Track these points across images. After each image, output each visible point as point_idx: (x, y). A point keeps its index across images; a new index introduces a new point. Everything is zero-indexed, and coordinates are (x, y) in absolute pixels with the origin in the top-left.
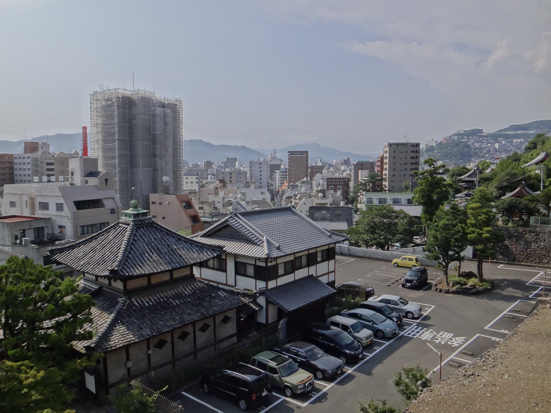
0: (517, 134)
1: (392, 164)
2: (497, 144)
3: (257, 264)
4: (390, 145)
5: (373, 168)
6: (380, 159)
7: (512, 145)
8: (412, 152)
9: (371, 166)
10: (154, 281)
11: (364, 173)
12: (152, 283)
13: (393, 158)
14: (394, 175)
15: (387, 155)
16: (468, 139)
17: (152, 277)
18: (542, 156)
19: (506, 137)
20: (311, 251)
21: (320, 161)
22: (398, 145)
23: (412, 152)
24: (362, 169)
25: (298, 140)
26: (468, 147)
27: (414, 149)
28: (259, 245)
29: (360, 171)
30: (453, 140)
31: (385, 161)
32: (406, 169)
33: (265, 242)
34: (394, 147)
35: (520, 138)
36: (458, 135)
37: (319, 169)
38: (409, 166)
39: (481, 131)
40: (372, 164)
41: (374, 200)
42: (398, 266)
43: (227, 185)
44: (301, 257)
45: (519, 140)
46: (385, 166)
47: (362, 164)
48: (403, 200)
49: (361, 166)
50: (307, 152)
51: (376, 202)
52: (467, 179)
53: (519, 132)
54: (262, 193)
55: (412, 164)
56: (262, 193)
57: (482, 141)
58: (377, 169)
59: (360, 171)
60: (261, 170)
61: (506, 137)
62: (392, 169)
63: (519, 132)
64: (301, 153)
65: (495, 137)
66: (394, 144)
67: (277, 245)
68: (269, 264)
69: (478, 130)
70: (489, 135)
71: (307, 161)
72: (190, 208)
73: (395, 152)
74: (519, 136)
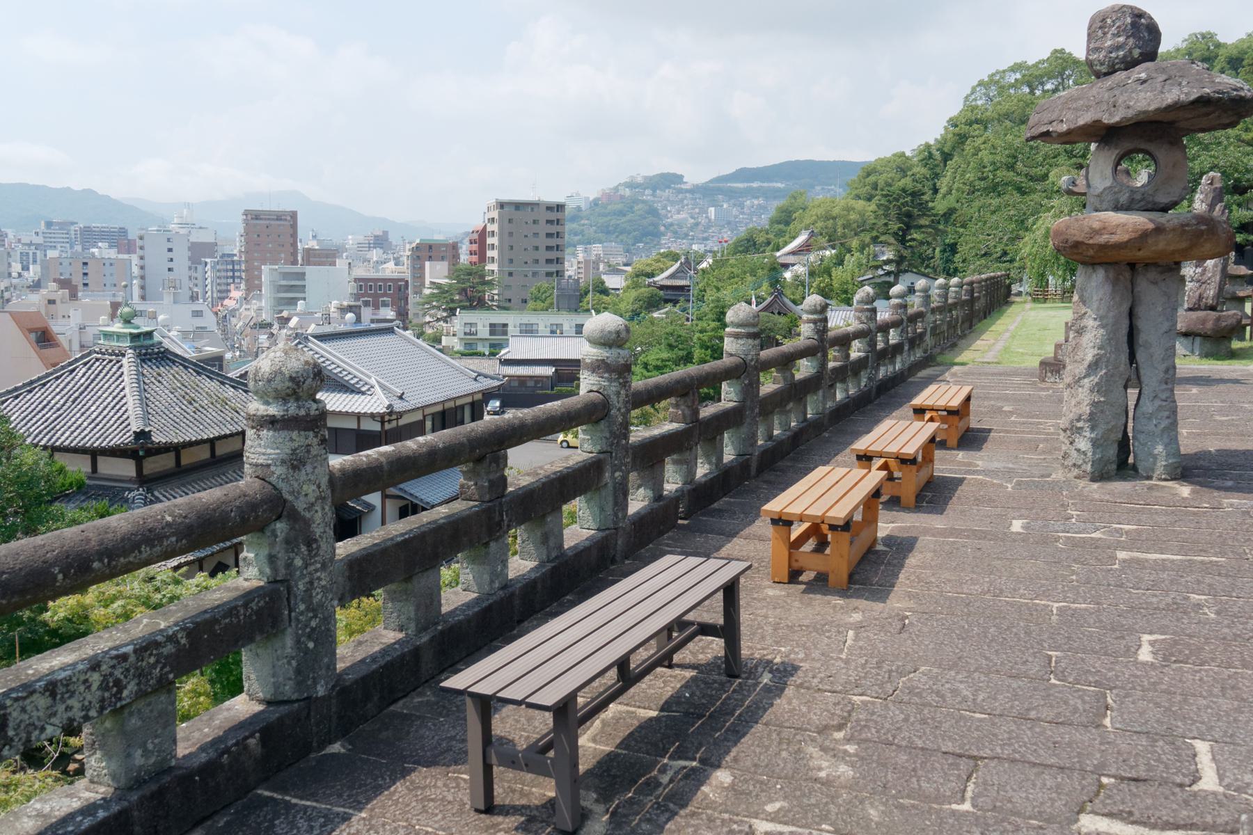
0: (751, 189)
1: (508, 248)
2: (712, 209)
3: (362, 427)
4: (502, 205)
5: (456, 256)
6: (476, 236)
7: (743, 213)
8: (548, 222)
9: (446, 251)
10: (187, 458)
11: (438, 267)
12: (145, 472)
13: (508, 234)
14: (511, 274)
15: (494, 227)
16: (654, 195)
17: (218, 443)
18: (802, 238)
19: (732, 194)
20: (448, 405)
21: (314, 237)
22: (518, 206)
23: (548, 222)
24: (430, 258)
25: (269, 188)
26: (653, 212)
27: (553, 216)
28: (363, 393)
29: (427, 264)
30: (622, 197)
31: (489, 241)
32: (537, 261)
33: (377, 386)
34: (512, 210)
35: (757, 198)
36: (631, 185)
37: (325, 256)
38: (543, 255)
39: (678, 178)
40: (455, 247)
41: (480, 327)
42: (569, 447)
43: (80, 294)
44: (462, 407)
45: (756, 202)
46: (490, 254)
47: (430, 247)
48: (541, 328)
49: (426, 251)
50: (294, 215)
51: (484, 332)
52: (669, 283)
53: (755, 185)
54: (197, 314)
55: (549, 248)
56: (197, 314)
57: (682, 201)
58: (464, 258)
59: (427, 264)
60: (170, 255)
61: (732, 194)
62: (508, 260)
63: (755, 185)
64: (279, 216)
65: (710, 191)
66: (510, 204)
67: (399, 392)
68: (387, 426)
69: (675, 175)
70: (695, 190)
71: (294, 235)
72: (52, 346)
73: (510, 221)
74: (753, 193)
